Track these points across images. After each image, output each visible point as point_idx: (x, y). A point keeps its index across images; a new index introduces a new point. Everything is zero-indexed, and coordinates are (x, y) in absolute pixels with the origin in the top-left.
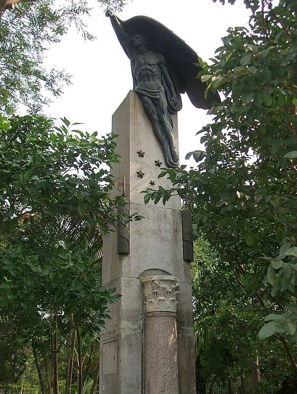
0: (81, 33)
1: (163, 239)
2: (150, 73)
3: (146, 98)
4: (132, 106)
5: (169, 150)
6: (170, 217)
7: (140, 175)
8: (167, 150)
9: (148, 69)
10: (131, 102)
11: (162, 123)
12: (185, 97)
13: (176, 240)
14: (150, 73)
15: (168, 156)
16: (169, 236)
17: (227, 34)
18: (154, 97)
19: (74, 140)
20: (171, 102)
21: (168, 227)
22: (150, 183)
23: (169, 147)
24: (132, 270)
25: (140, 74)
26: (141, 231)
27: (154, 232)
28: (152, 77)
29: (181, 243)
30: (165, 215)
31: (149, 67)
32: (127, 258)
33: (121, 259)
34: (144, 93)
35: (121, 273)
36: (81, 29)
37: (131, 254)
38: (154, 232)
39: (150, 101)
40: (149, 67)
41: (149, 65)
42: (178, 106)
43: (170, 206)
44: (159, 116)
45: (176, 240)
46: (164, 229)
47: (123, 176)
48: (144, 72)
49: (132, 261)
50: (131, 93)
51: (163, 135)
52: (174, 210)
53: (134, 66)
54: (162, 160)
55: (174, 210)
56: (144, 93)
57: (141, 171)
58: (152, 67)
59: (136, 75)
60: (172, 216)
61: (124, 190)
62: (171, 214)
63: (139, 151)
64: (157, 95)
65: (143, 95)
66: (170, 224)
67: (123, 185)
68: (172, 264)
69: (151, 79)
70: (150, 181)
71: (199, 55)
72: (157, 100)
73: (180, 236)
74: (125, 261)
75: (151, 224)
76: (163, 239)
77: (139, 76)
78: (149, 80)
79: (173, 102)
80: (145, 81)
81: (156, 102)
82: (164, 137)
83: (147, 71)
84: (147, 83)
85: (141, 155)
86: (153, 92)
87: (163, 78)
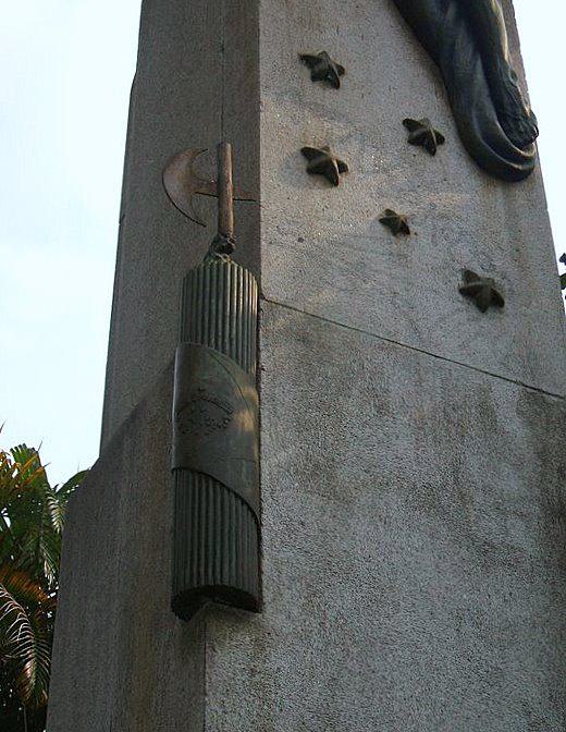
1: (486, 550)
5: (480, 77)
7: (322, 168)
8: (472, 76)
19: (52, 529)
21: (511, 484)
22: (383, 221)
23: (479, 63)
26: (343, 474)
30: (486, 411)
32: (244, 638)
33: (194, 648)
38: (427, 500)
43: (512, 365)
46: (487, 490)
47: (220, 147)
49: (278, 661)
57: (327, 149)
62: (519, 412)
66: (518, 466)
70: (378, 212)
71: (521, 48)
74: (229, 657)
75: (404, 445)
76: (486, 550)
82: (451, 11)
85: (325, 73)
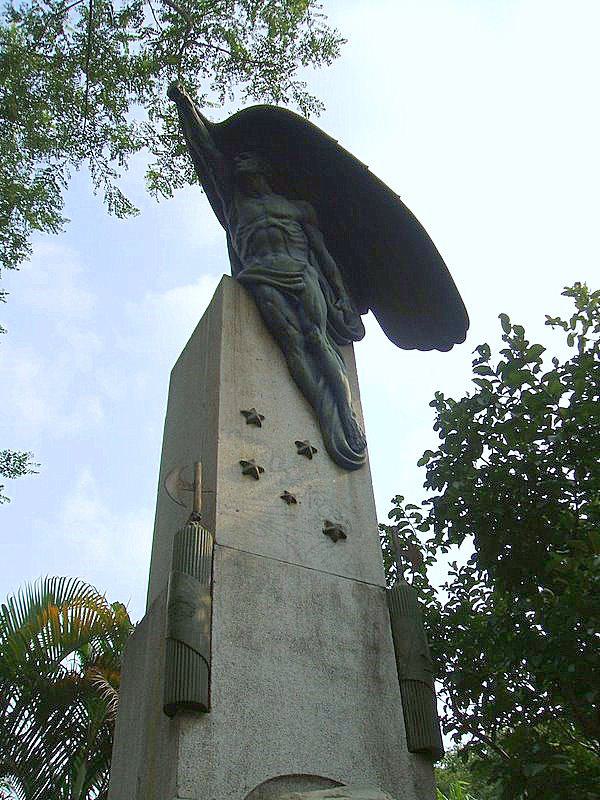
0: (102, 191)
1: (332, 672)
2: (279, 233)
3: (268, 290)
4: (228, 307)
5: (336, 417)
6: (350, 603)
7: (250, 471)
8: (331, 418)
9: (275, 226)
10: (226, 299)
11: (313, 349)
12: (369, 320)
13: (377, 679)
14: (279, 233)
15: (336, 434)
16: (353, 662)
17: (424, 470)
18: (292, 286)
20: (335, 310)
21: (348, 634)
23: (336, 409)
24: (220, 775)
25: (251, 240)
27: (301, 646)
28: (283, 244)
29: (394, 692)
30: (336, 597)
31: (275, 221)
32: (200, 727)
33: (174, 733)
34: (263, 278)
35: (173, 779)
36: (103, 184)
37: (215, 714)
38: (301, 646)
39: (279, 297)
40: (275, 221)
41: (276, 216)
42: (359, 333)
44: (305, 331)
45: (377, 679)
47: (196, 464)
48: (263, 232)
49: (219, 738)
50: (226, 280)
51: (318, 382)
52: (362, 585)
53: (234, 231)
54: (314, 441)
55: (362, 585)
56: (263, 278)
58: (284, 221)
59: (240, 249)
60: (359, 601)
61: (195, 502)
63: (248, 408)
64: (300, 282)
65: (261, 283)
66: (351, 625)
67: (195, 489)
68: (368, 763)
69: (282, 249)
72: (300, 292)
73: (389, 668)
74: (192, 737)
76: (332, 672)
77: (247, 243)
78: (275, 251)
79: (341, 312)
80: (265, 254)
81: (296, 298)
82: (321, 383)
83: (272, 229)
84: (270, 257)
85: (254, 420)
86: (287, 276)
87: (312, 255)
